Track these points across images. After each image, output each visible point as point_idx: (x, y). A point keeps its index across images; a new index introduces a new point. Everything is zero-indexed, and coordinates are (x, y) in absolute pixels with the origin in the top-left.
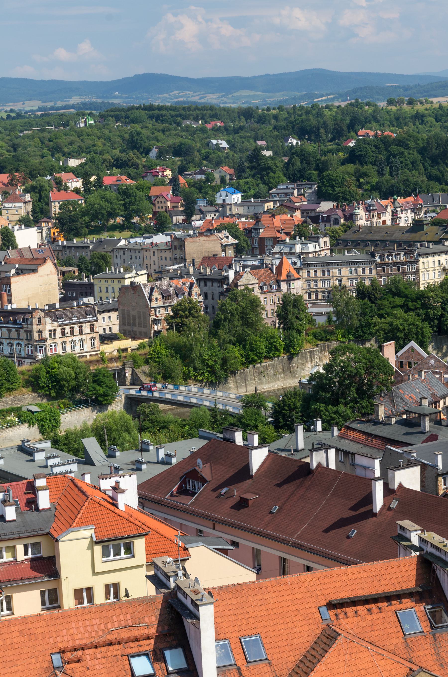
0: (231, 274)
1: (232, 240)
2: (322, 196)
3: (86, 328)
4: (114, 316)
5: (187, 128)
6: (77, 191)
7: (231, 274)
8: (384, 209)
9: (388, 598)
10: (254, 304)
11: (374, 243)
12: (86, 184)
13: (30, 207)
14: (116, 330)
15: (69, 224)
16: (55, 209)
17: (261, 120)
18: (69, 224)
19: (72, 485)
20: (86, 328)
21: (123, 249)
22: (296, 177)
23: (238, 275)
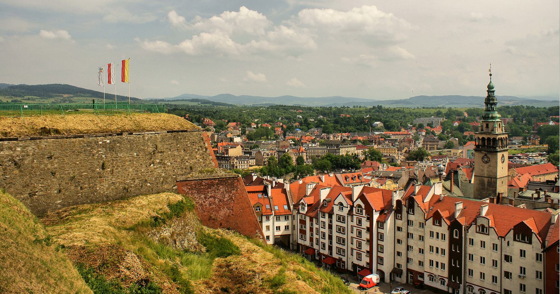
0: (286, 150)
1: (293, 143)
2: (324, 132)
3: (246, 162)
4: (254, 160)
5: (291, 112)
6: (254, 128)
7: (286, 150)
8: (339, 136)
9: (257, 192)
10: (289, 158)
11: (328, 144)
12: (257, 126)
13: (241, 132)
14: (254, 164)
15: (250, 138)
16: (247, 132)
17: (314, 111)
18: (250, 138)
19: (106, 69)
20: (246, 162)
21: (263, 144)
22: (317, 126)
23: (288, 151)
